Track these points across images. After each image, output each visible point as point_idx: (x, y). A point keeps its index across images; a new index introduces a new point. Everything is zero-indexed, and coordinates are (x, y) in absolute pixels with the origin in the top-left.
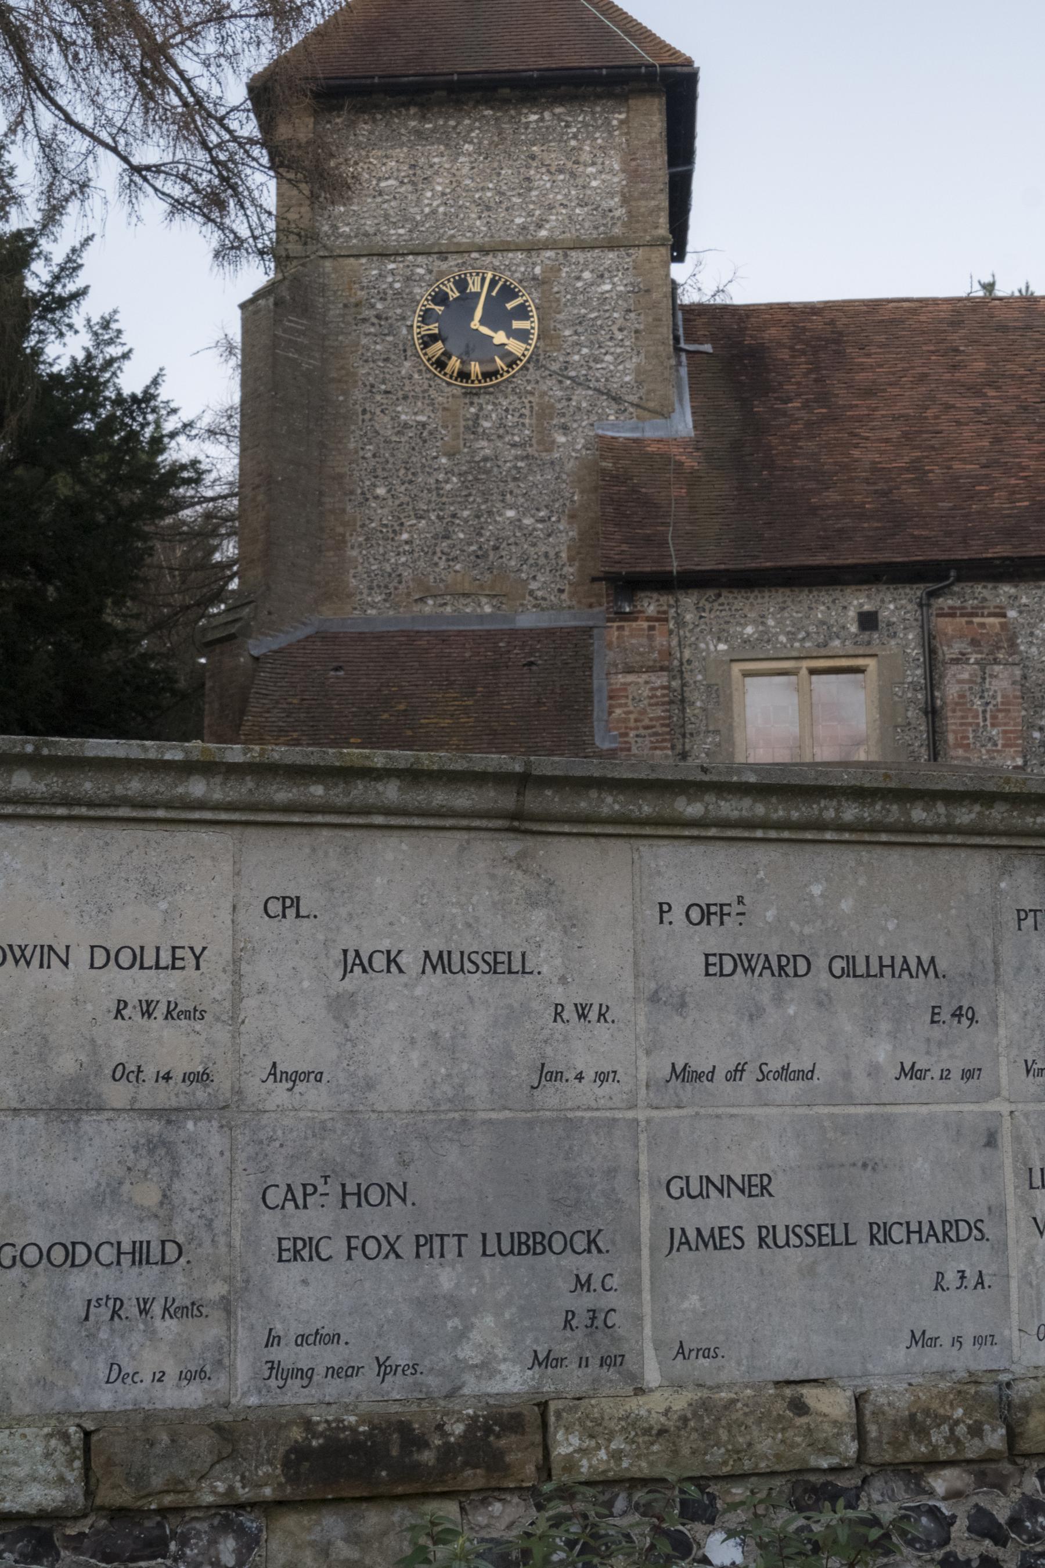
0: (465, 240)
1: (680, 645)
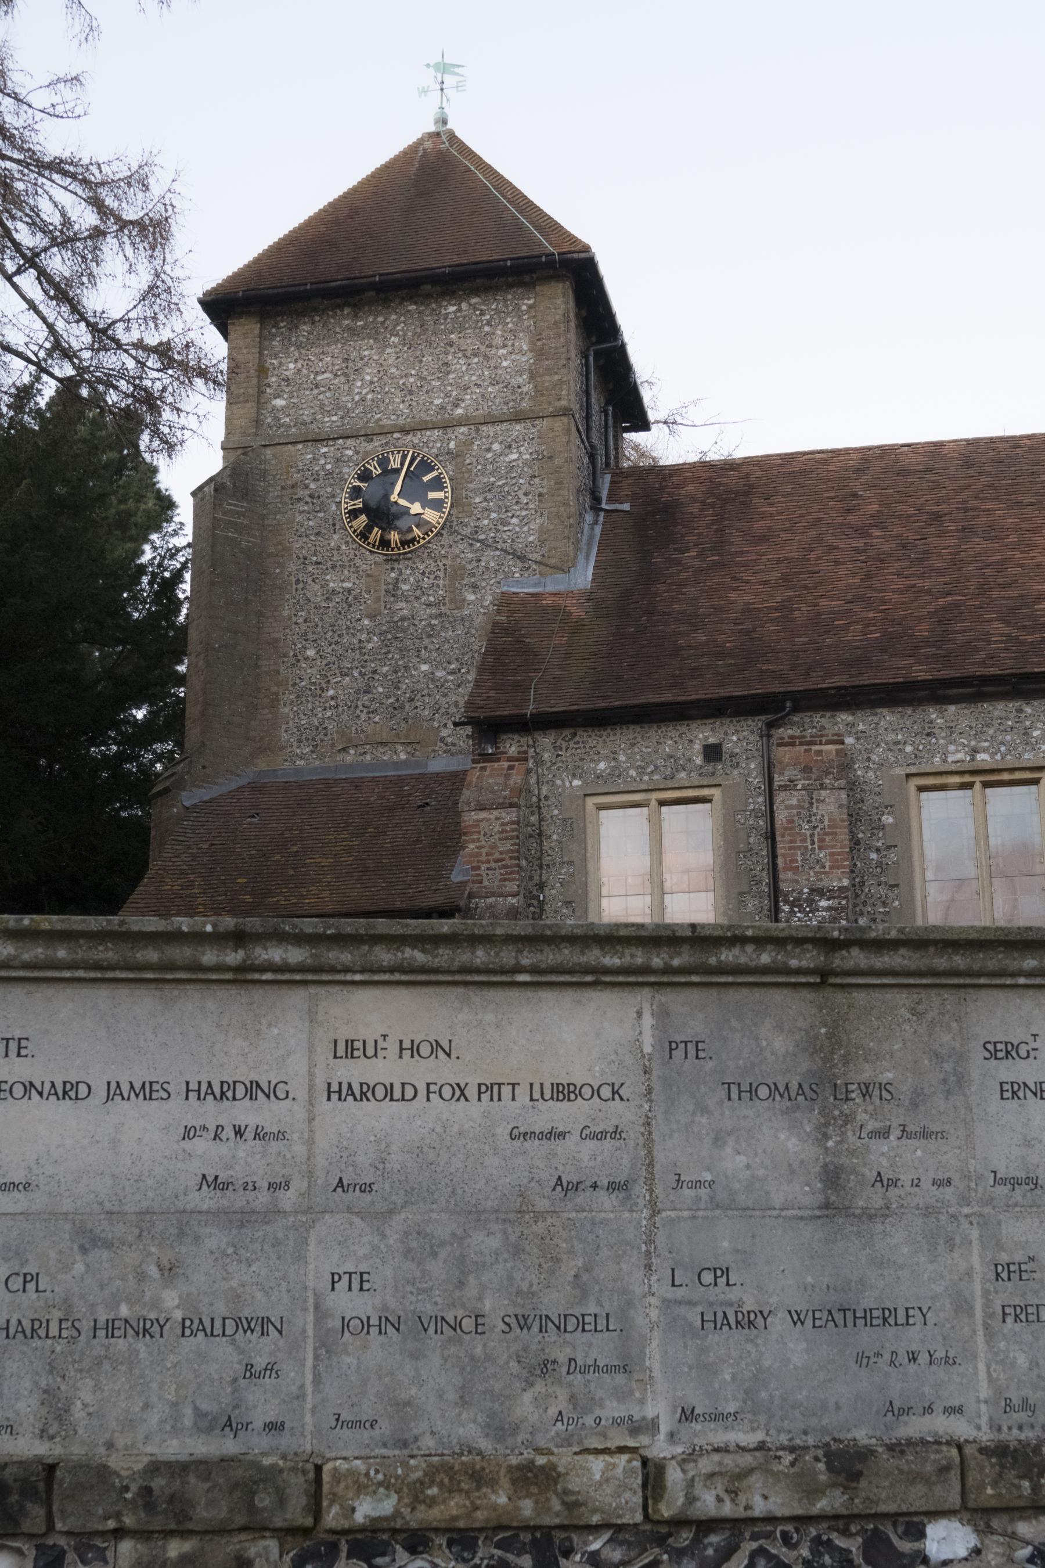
0: (390, 422)
1: (538, 782)
